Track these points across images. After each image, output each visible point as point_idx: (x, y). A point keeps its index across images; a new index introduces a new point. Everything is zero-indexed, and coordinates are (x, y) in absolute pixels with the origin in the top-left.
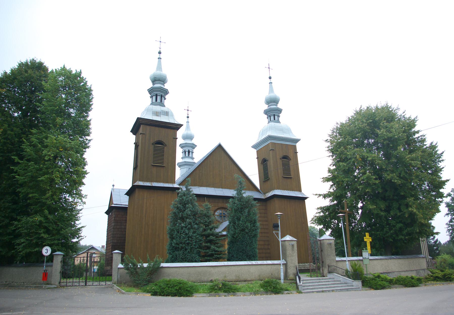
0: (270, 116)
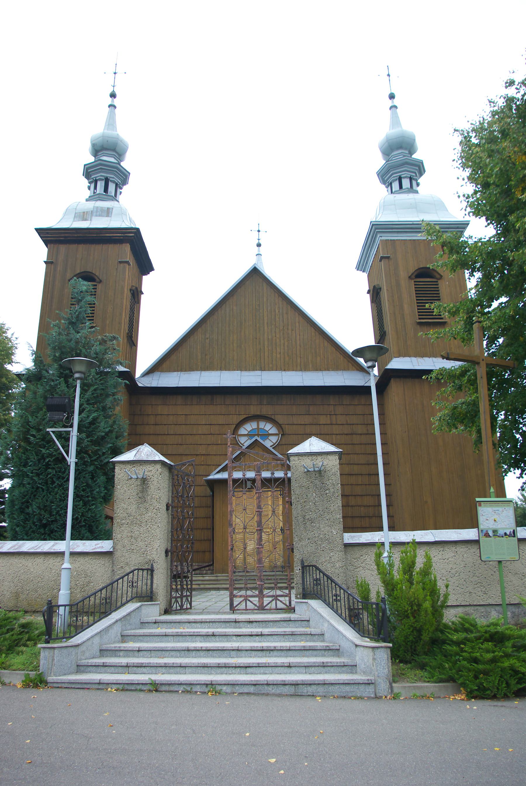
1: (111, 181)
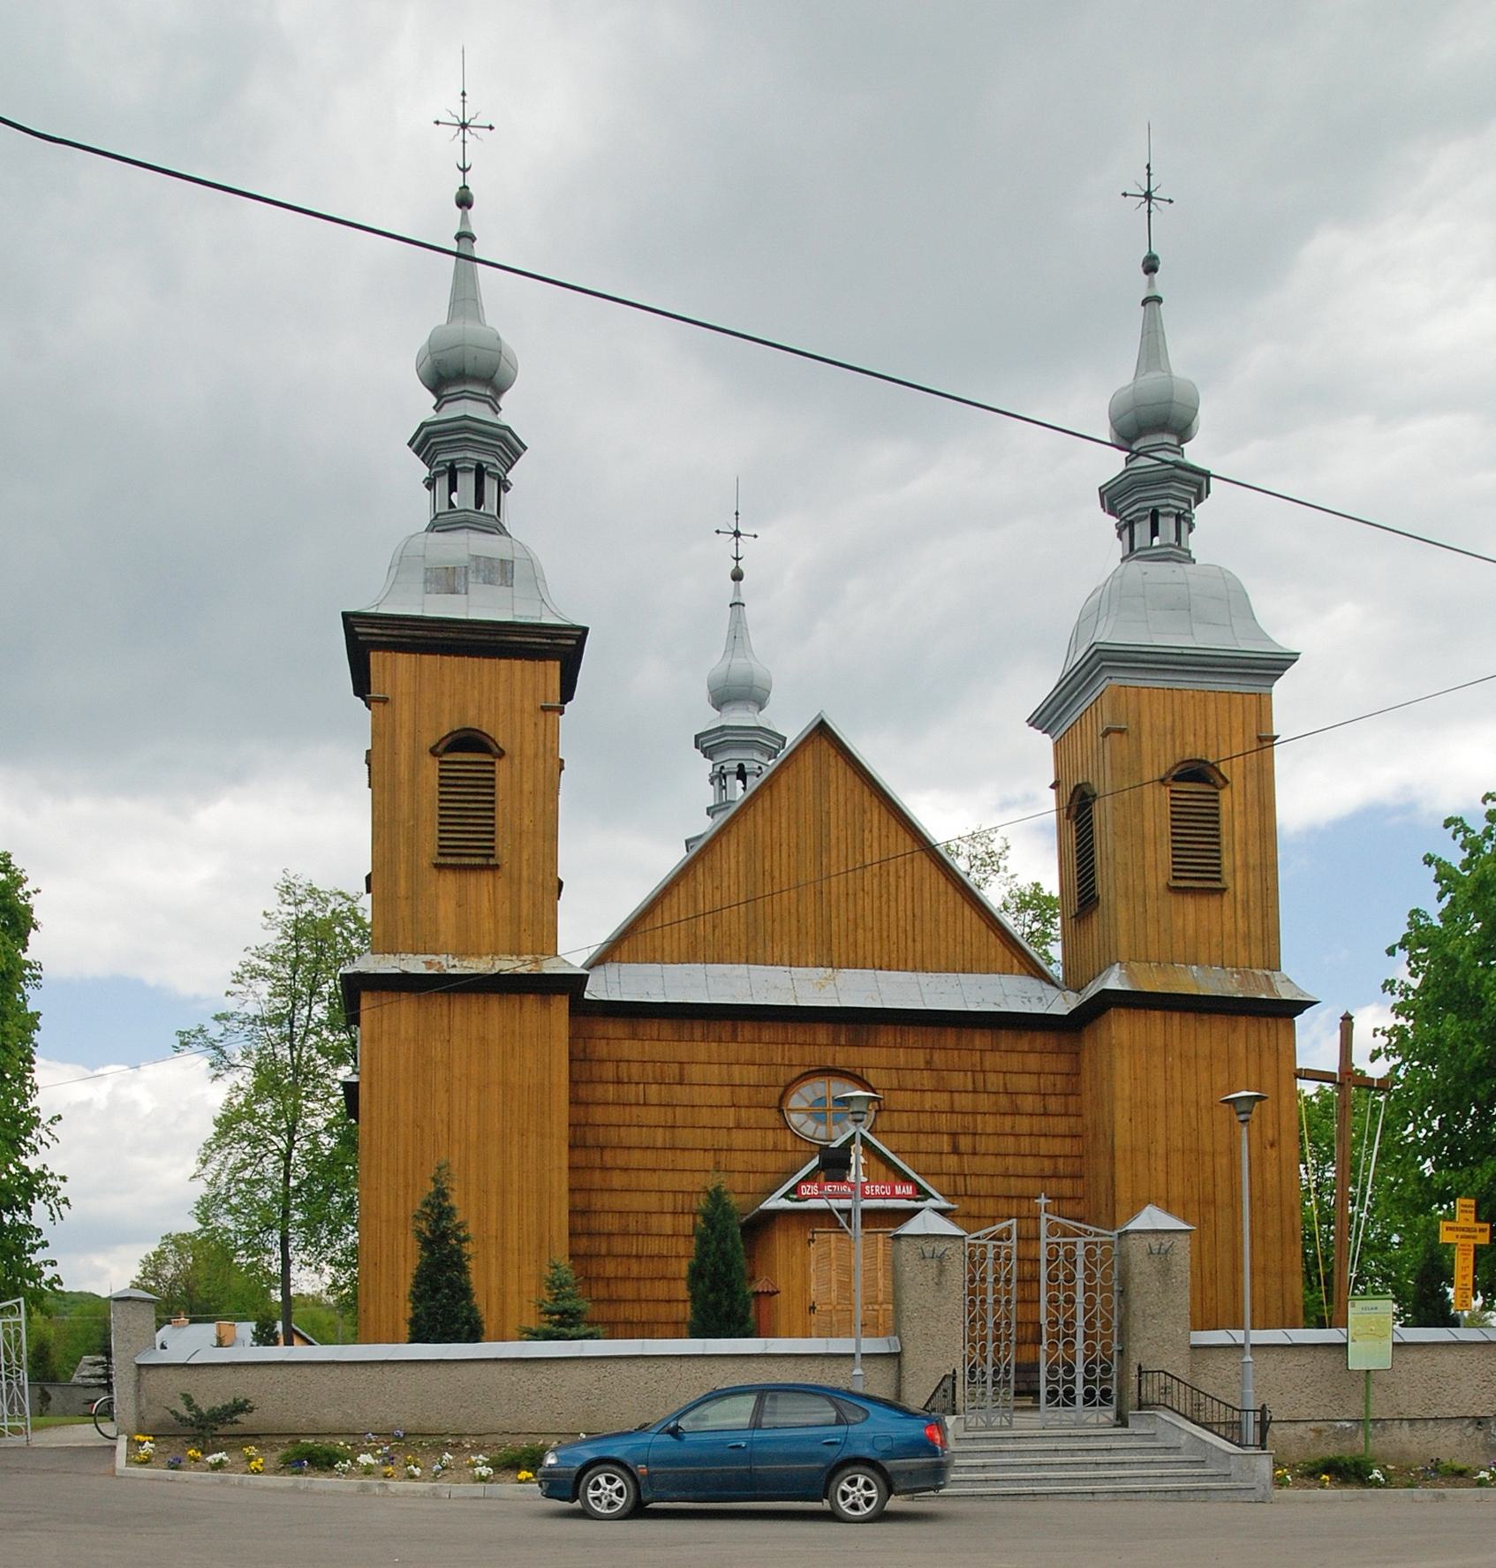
0: (1131, 524)
1: (490, 474)
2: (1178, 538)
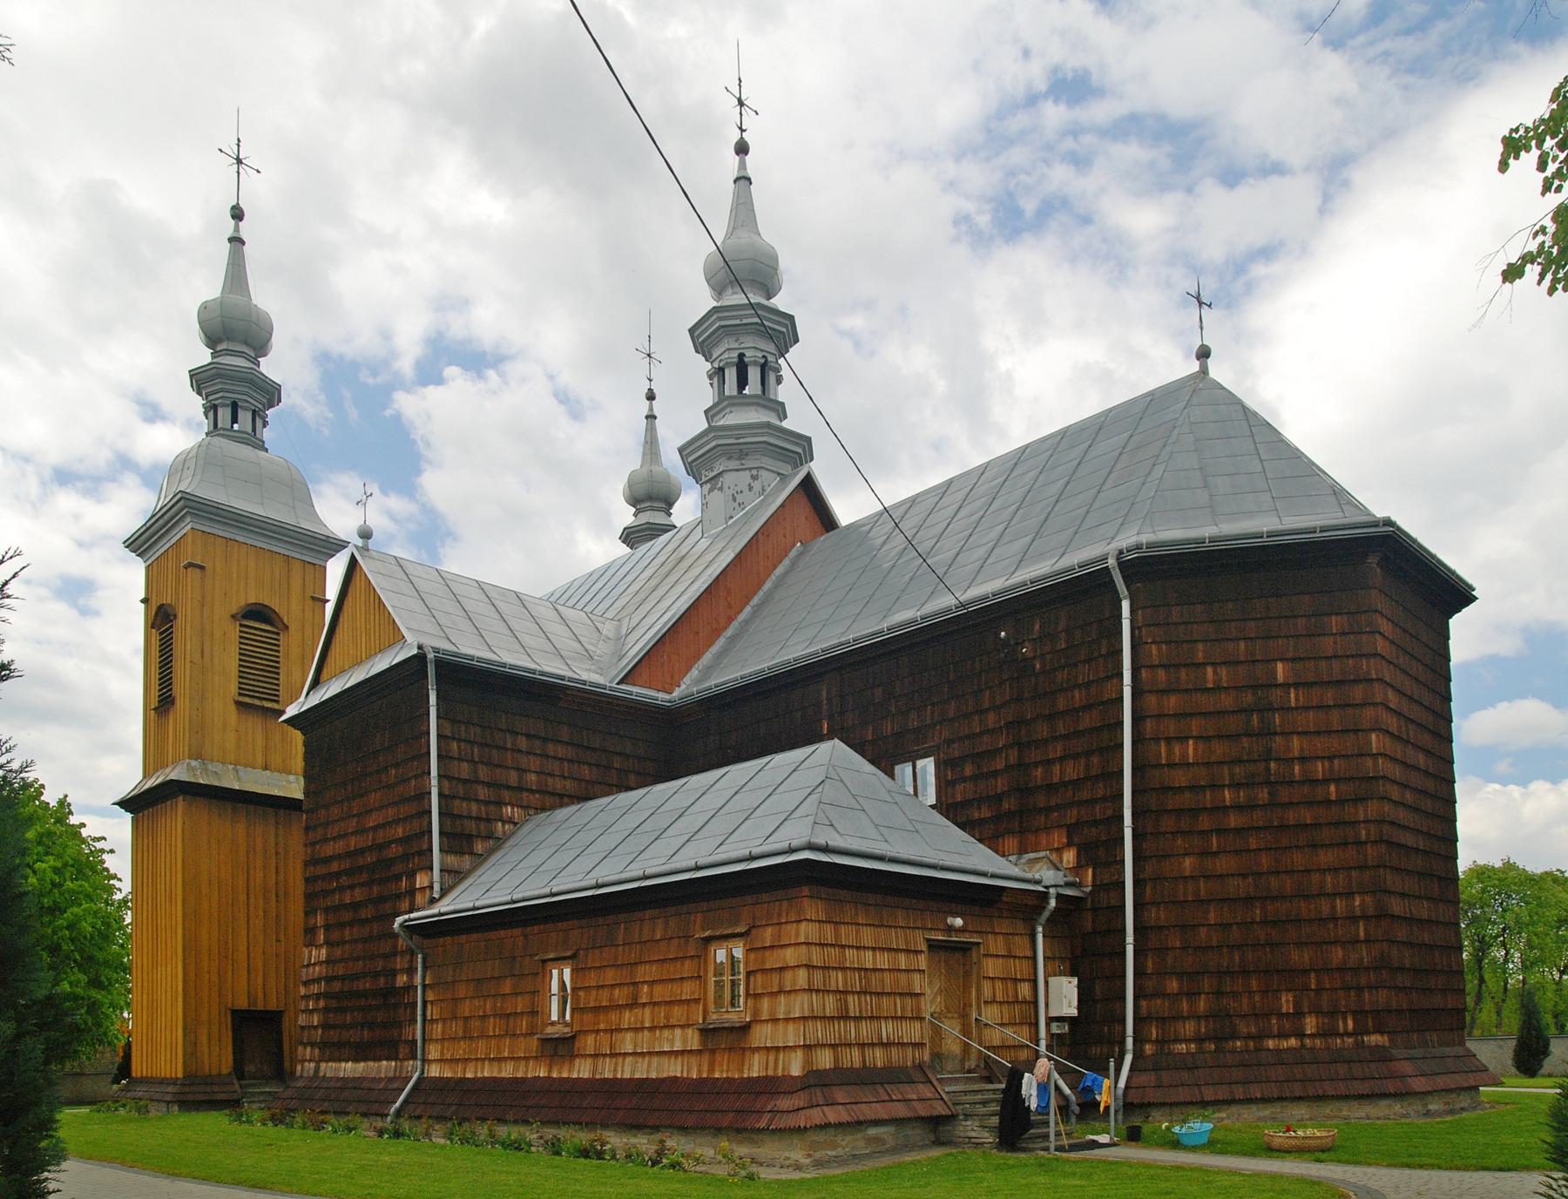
0: (215, 408)
2: (254, 430)
